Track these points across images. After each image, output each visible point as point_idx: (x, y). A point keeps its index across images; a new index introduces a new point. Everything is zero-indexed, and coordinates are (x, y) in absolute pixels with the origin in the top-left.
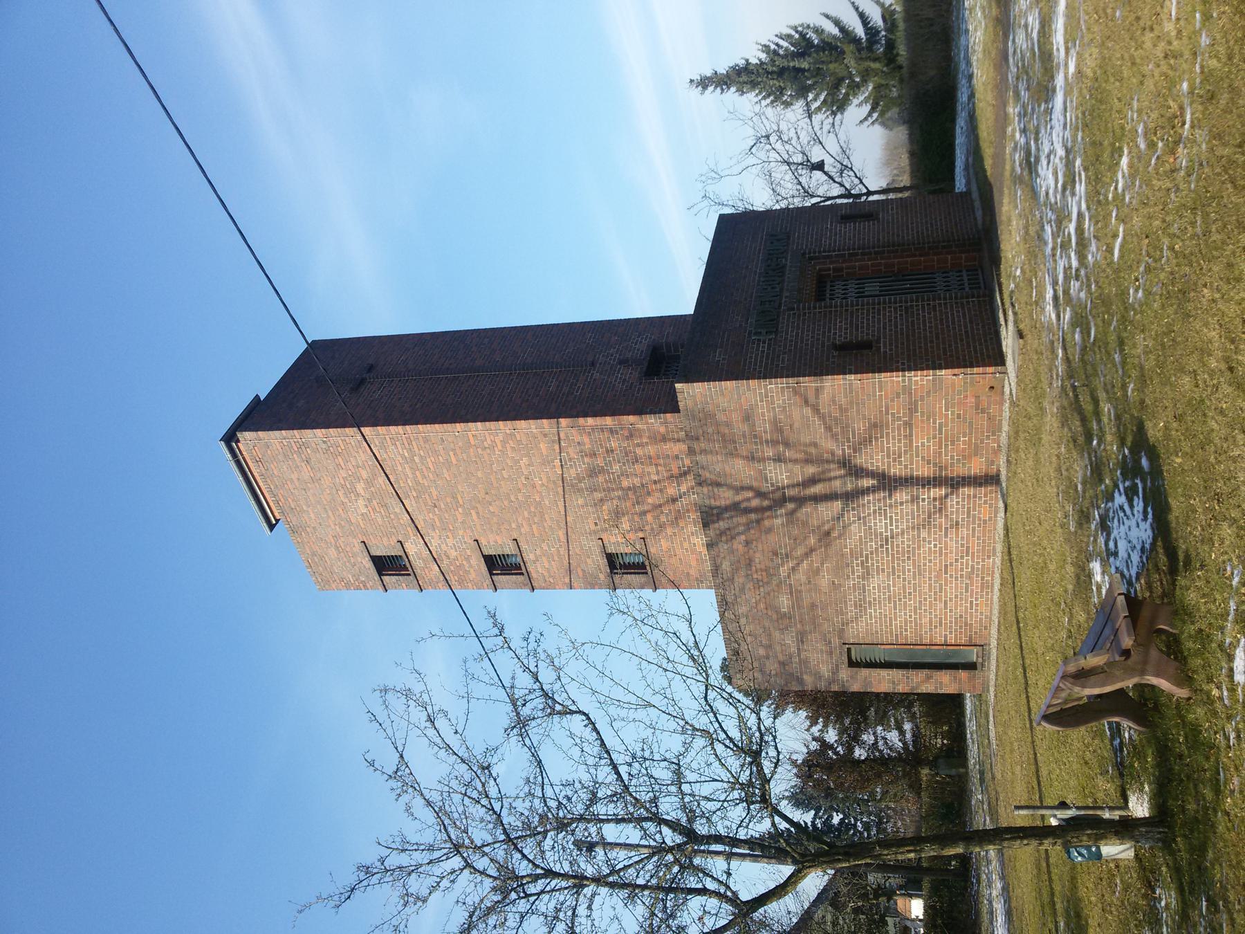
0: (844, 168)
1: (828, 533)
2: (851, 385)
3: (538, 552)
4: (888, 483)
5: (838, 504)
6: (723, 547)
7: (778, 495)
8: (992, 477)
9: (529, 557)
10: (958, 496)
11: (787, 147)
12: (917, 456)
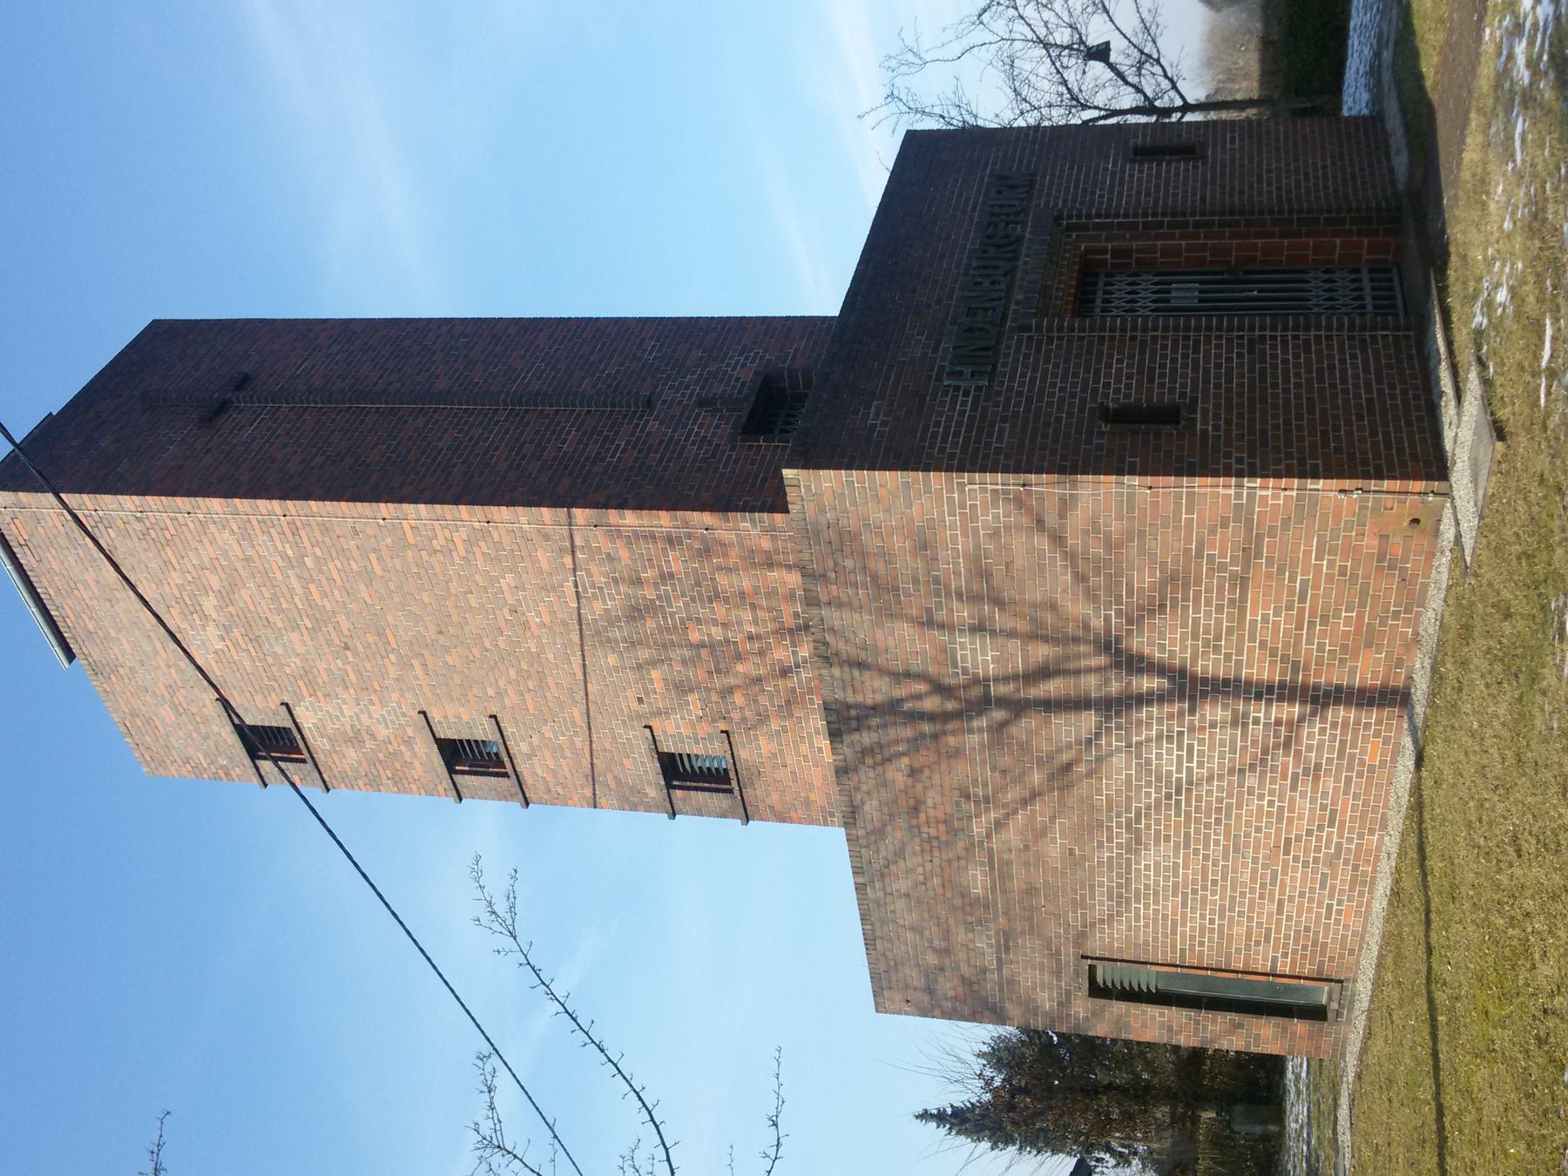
0: (1145, 59)
1: (1068, 767)
2: (1131, 497)
3: (535, 740)
4: (1189, 688)
5: (1089, 719)
6: (866, 777)
7: (976, 692)
8: (1395, 691)
9: (519, 748)
10: (1323, 720)
11: (1046, 14)
12: (1252, 639)
